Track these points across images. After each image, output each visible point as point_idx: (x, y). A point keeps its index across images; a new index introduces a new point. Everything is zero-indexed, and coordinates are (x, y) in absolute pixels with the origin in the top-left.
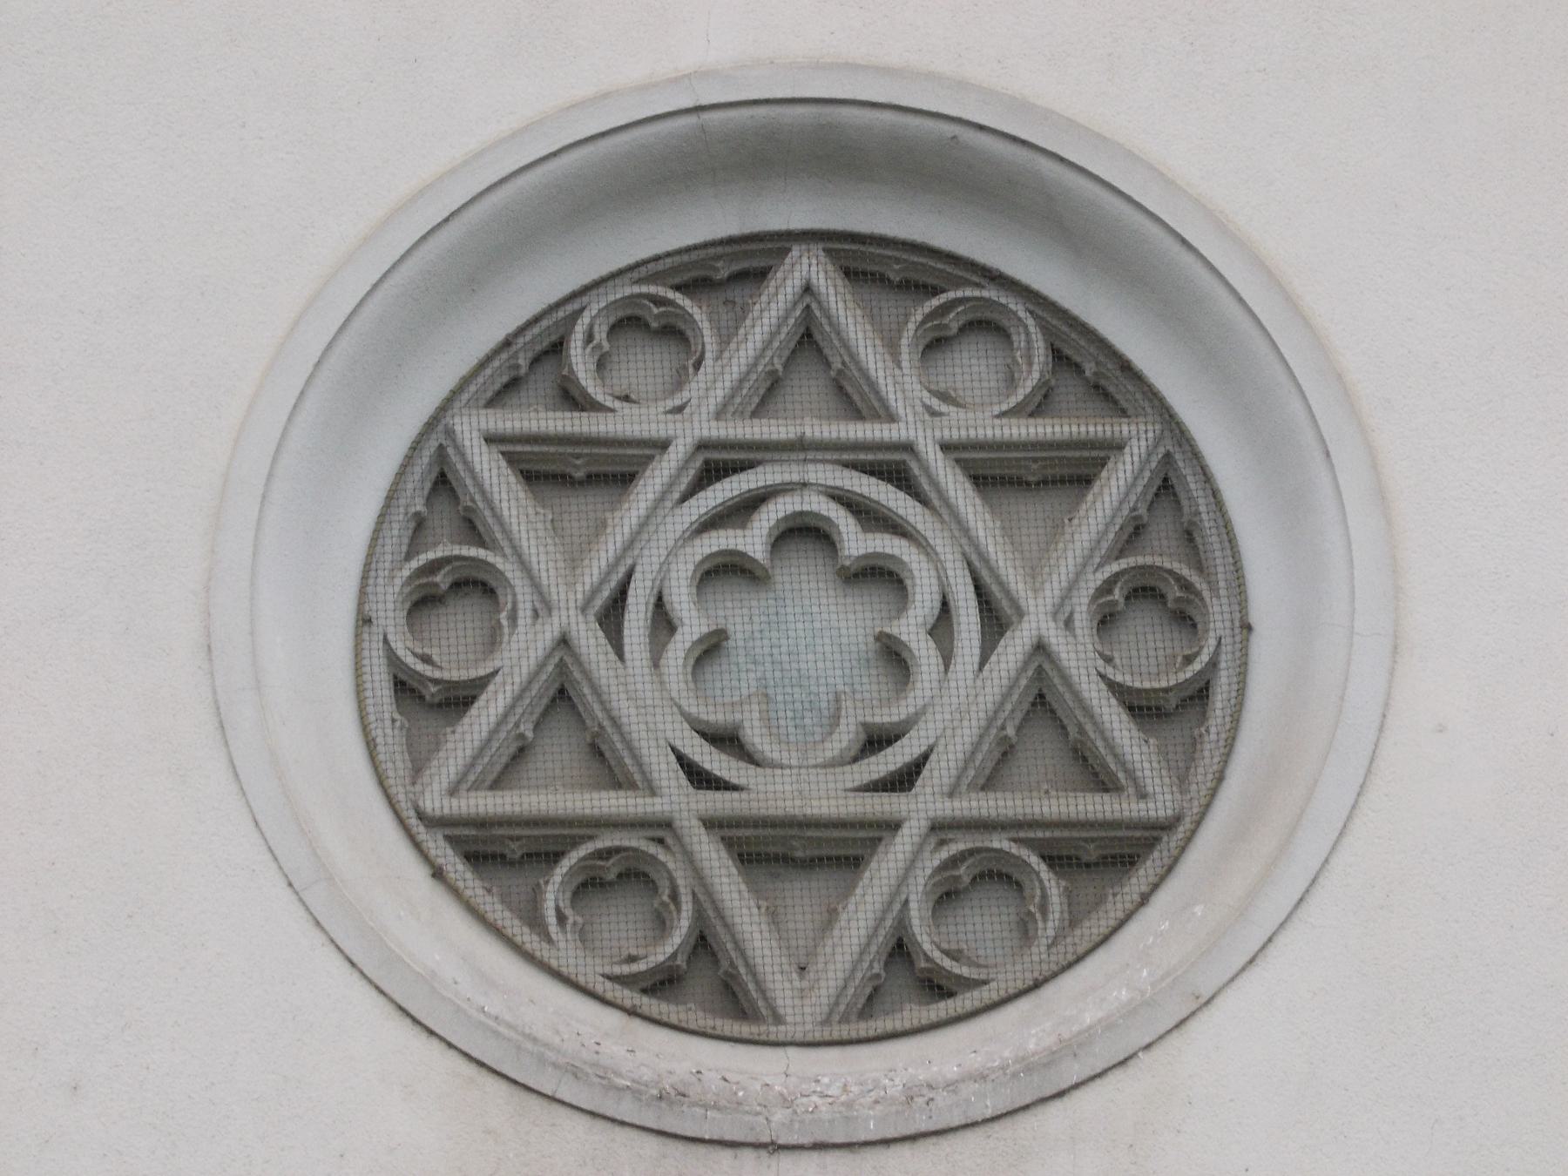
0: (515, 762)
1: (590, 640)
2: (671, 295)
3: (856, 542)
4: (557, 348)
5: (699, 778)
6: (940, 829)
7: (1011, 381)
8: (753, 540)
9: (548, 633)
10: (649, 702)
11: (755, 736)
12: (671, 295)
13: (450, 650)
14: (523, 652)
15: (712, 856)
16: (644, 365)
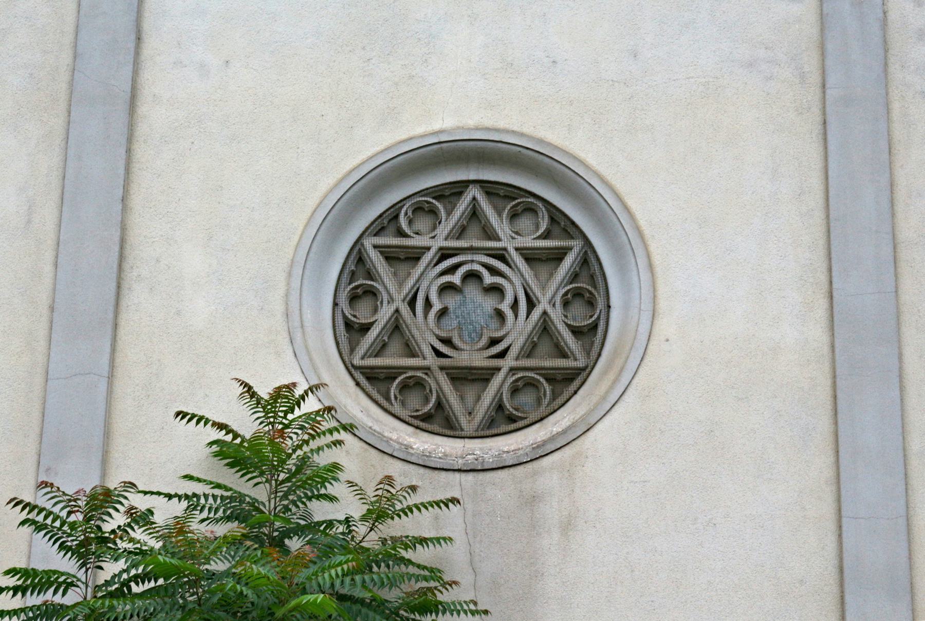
0: (380, 349)
1: (405, 310)
2: (431, 200)
3: (488, 279)
4: (396, 217)
5: (439, 354)
6: (513, 370)
7: (537, 227)
8: (456, 278)
9: (392, 308)
10: (424, 330)
11: (456, 341)
12: (431, 200)
13: (362, 314)
14: (385, 314)
15: (443, 378)
16: (423, 223)
